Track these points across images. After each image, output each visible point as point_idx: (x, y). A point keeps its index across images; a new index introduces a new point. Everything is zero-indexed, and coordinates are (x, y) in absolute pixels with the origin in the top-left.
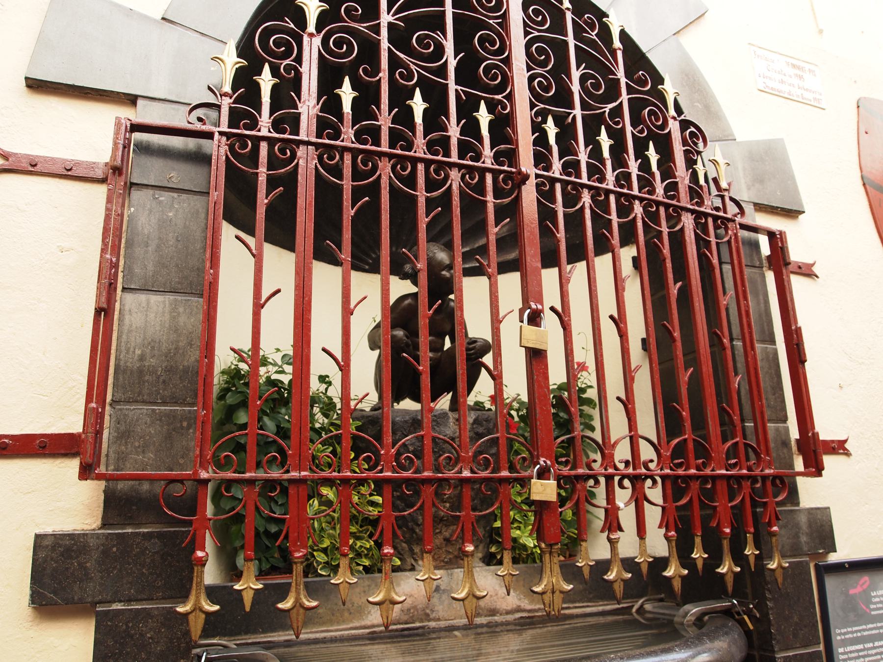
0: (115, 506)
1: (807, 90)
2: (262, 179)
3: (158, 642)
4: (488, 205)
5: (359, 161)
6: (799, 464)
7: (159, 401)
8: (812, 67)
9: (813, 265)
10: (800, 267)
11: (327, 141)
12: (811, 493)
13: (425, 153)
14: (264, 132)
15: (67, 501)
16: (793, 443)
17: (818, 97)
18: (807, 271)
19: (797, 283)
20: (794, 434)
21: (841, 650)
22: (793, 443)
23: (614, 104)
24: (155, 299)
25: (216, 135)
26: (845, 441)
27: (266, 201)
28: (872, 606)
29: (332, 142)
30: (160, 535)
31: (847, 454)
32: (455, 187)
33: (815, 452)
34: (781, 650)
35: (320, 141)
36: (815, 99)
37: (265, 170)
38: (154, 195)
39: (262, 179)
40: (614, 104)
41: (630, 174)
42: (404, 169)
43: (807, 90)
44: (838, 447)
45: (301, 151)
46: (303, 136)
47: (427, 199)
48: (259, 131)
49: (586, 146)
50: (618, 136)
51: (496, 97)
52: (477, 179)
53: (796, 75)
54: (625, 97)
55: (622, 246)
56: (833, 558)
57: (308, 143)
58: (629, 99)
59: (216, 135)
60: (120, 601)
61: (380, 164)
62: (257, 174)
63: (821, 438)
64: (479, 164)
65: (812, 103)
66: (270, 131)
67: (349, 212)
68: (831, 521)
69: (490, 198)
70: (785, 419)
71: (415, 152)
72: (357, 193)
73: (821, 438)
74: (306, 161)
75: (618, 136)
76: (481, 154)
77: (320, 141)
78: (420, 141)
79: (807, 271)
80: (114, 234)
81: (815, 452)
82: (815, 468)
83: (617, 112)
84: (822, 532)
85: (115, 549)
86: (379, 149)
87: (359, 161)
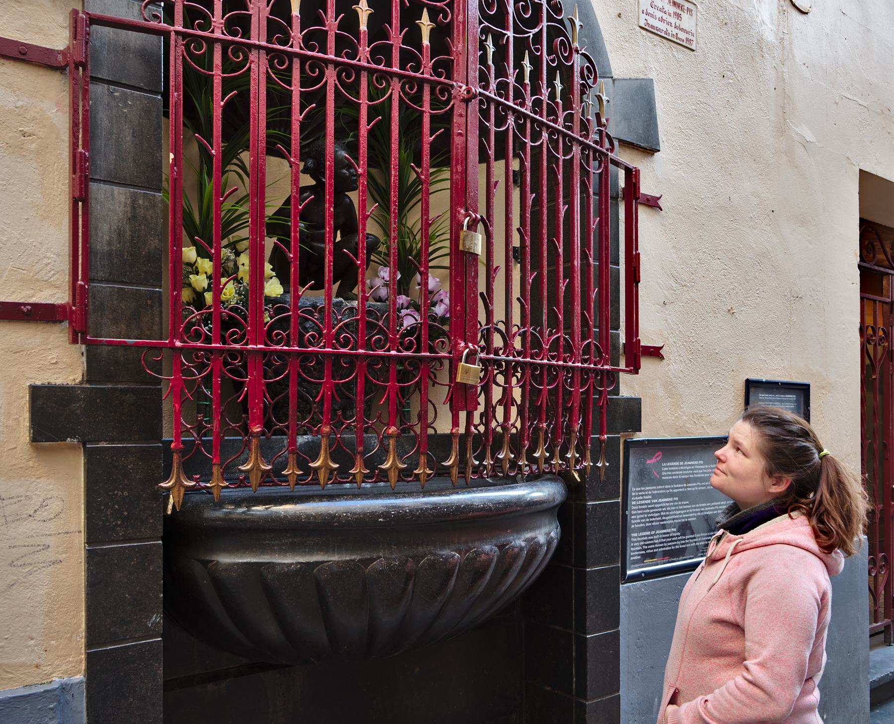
0: (96, 368)
1: (682, 30)
2: (217, 82)
3: (137, 472)
4: (425, 115)
5: (307, 67)
6: (622, 365)
7: (134, 281)
8: (691, 6)
9: (659, 198)
10: (648, 200)
11: (346, 60)
12: (629, 386)
13: (301, 48)
14: (218, 34)
15: (60, 361)
16: (621, 346)
17: (690, 37)
18: (653, 203)
19: (644, 215)
20: (623, 340)
21: (634, 503)
22: (621, 346)
23: (537, 30)
24: (117, 190)
25: (173, 34)
26: (661, 348)
27: (222, 103)
28: (664, 473)
29: (282, 48)
30: (133, 391)
31: (662, 358)
32: (396, 97)
33: (637, 354)
34: (591, 500)
35: (270, 46)
36: (687, 40)
37: (220, 72)
38: (108, 90)
39: (217, 82)
40: (537, 30)
41: (508, 83)
42: (348, 76)
43: (682, 30)
44: (655, 353)
45: (253, 55)
46: (254, 41)
47: (369, 106)
48: (213, 32)
49: (515, 69)
50: (536, 62)
51: (438, 4)
52: (415, 90)
53: (675, 13)
54: (545, 24)
55: (495, 160)
56: (639, 437)
57: (259, 47)
58: (548, 26)
59: (173, 34)
60: (106, 441)
61: (327, 71)
62: (213, 75)
63: (642, 344)
64: (418, 75)
65: (684, 44)
66: (223, 33)
67: (297, 117)
68: (640, 409)
69: (426, 107)
70: (617, 328)
71: (422, 73)
72: (306, 98)
73: (642, 344)
74: (258, 67)
75: (536, 62)
76: (210, 21)
77: (339, 59)
78: (364, 50)
79: (653, 203)
80: (83, 126)
81: (637, 354)
82: (634, 367)
83: (538, 37)
84: (632, 414)
85: (98, 401)
86: (326, 56)
87: (307, 67)
